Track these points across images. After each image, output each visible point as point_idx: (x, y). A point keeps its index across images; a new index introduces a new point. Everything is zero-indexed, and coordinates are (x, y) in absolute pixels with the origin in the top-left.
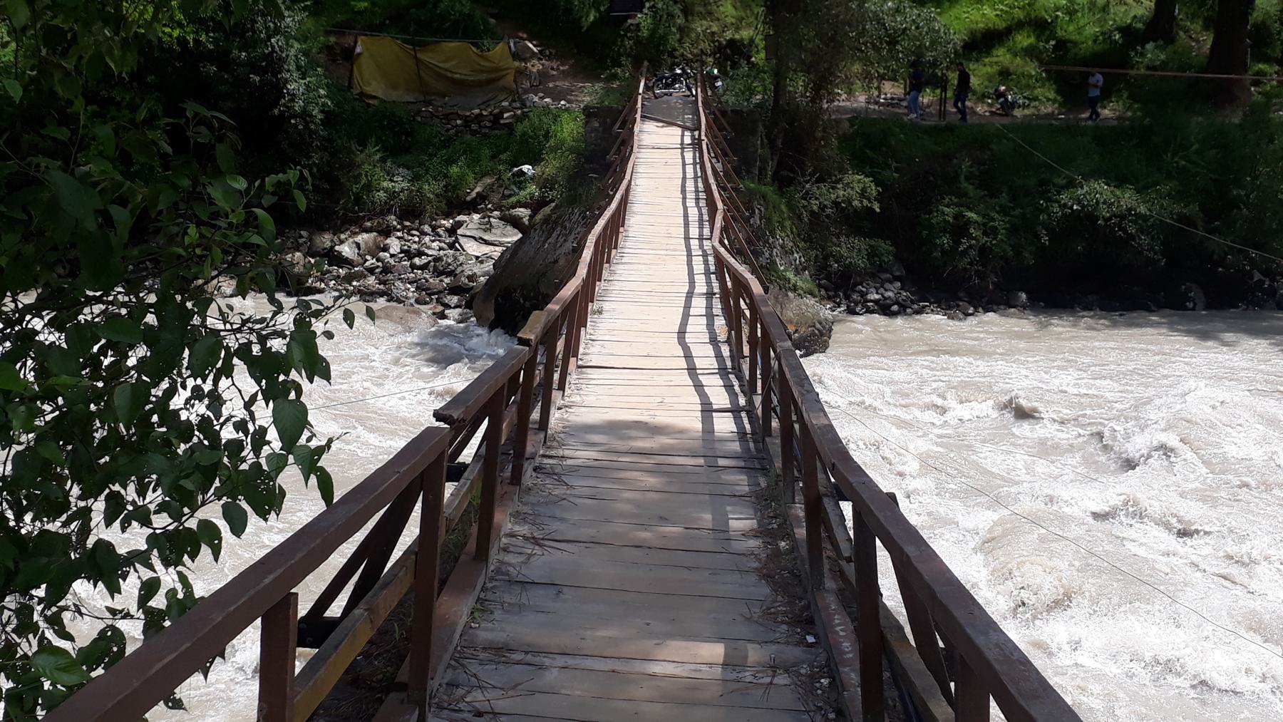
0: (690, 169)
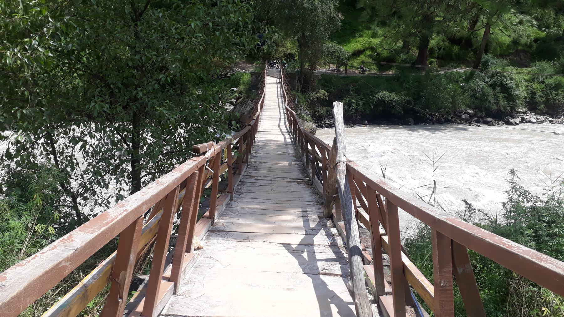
0: (279, 89)
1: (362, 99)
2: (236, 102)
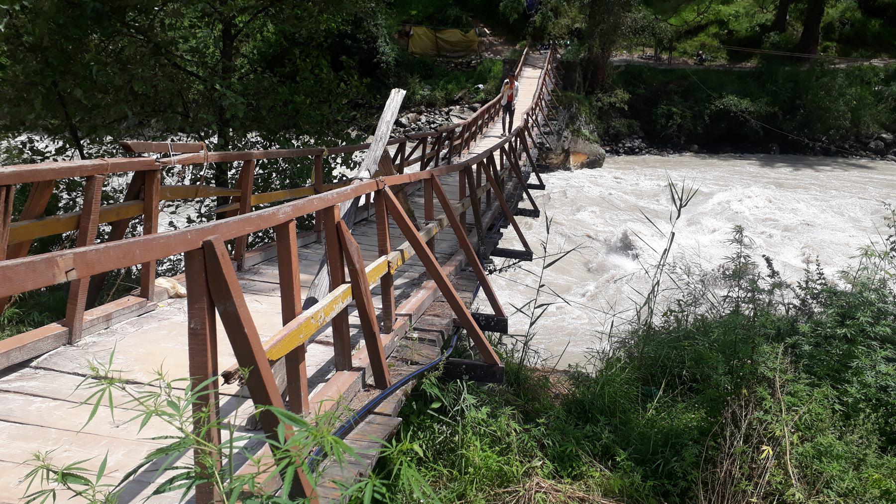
1: (690, 108)
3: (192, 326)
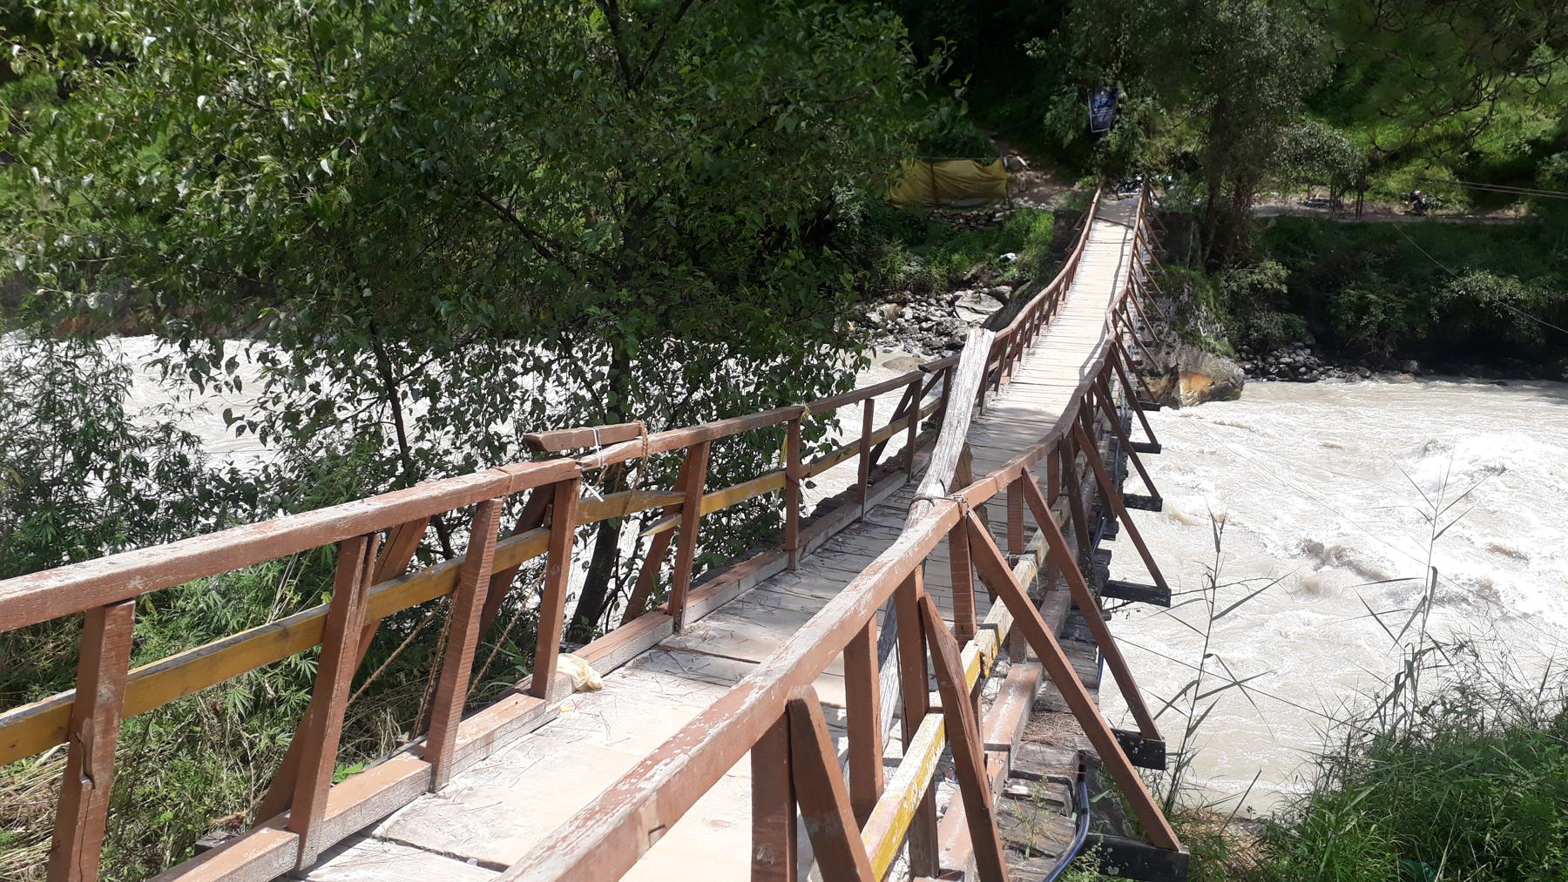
1: (1402, 294)
2: (1012, 293)
3: (759, 857)
